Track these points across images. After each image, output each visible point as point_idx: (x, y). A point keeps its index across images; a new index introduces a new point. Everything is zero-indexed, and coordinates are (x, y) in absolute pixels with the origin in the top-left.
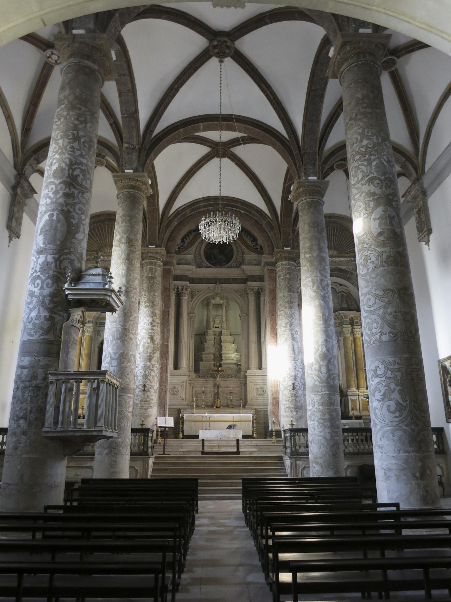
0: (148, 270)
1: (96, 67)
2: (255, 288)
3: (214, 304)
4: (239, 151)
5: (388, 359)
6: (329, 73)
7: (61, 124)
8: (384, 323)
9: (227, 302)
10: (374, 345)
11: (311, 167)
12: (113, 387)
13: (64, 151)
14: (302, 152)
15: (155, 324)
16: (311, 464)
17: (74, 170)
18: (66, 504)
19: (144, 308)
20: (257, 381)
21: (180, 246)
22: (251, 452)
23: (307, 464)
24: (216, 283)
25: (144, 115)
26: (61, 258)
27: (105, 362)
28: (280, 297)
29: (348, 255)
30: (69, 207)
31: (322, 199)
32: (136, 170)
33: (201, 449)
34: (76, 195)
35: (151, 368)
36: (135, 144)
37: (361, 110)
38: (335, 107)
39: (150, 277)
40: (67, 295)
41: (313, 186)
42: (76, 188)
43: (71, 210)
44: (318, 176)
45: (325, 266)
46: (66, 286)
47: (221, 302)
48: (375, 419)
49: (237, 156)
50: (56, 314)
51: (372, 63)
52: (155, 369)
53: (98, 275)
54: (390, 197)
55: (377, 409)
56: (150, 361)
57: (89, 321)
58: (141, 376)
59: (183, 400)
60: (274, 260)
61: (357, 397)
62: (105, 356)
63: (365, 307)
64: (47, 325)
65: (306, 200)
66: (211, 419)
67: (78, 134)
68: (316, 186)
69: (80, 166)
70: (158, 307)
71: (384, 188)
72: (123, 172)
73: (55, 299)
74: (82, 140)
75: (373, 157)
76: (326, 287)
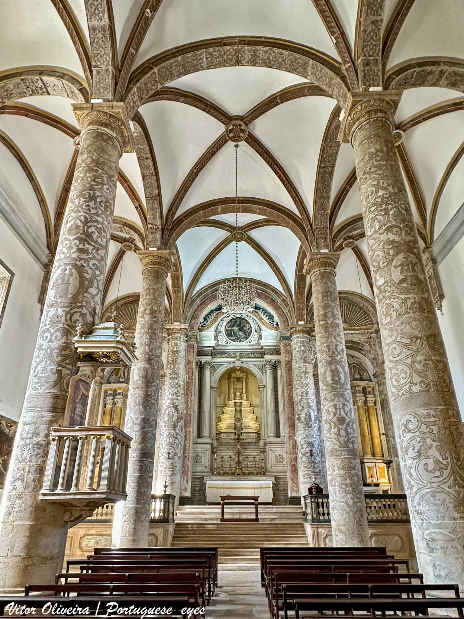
0: (173, 344)
1: (114, 135)
3: (235, 378)
4: (255, 234)
5: (421, 411)
6: (340, 138)
7: (78, 184)
8: (414, 373)
9: (247, 376)
10: (403, 397)
13: (80, 209)
14: (313, 228)
15: (179, 394)
16: (333, 533)
17: (89, 227)
18: (82, 572)
22: (272, 519)
23: (329, 532)
25: (167, 199)
26: (72, 312)
27: (127, 428)
28: (296, 368)
29: (359, 328)
30: (82, 262)
31: (335, 271)
33: (220, 516)
34: (90, 251)
35: (175, 436)
36: (158, 224)
37: (375, 163)
39: (175, 351)
40: (76, 349)
41: (325, 258)
42: (90, 244)
43: (85, 265)
45: (339, 332)
46: (76, 338)
47: (242, 375)
48: (410, 479)
50: (63, 367)
51: (384, 120)
52: (179, 437)
53: (110, 328)
54: (411, 244)
55: (412, 468)
56: (174, 430)
57: (119, 394)
63: (391, 357)
64: (54, 378)
67: (94, 194)
68: (328, 258)
69: (96, 224)
70: (183, 379)
71: (403, 235)
72: (147, 249)
73: (63, 352)
74: (98, 200)
75: (390, 207)
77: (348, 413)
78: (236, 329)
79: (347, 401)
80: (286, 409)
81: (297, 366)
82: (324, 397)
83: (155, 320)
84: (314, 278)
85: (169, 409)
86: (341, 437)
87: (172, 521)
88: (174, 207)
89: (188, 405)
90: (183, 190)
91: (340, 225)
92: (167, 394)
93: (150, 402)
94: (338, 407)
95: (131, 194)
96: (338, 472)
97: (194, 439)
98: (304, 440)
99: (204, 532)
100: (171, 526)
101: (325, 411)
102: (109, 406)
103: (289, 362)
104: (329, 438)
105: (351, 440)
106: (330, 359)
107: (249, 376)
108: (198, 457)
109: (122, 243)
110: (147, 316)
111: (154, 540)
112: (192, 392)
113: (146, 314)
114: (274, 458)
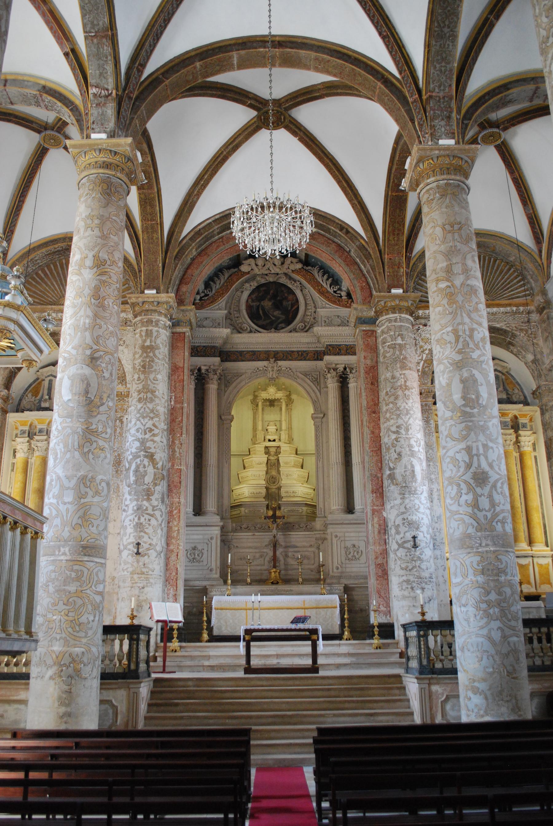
0: (143, 334)
2: (338, 366)
3: (266, 400)
9: (289, 396)
11: (443, 123)
12: (24, 533)
14: (424, 97)
15: (156, 431)
19: (138, 404)
20: (347, 534)
21: (203, 295)
24: (267, 359)
27: (51, 495)
28: (386, 379)
31: (467, 182)
32: (112, 135)
33: (243, 662)
35: (150, 511)
38: (483, 12)
39: (148, 347)
41: (448, 156)
44: (456, 137)
47: (280, 395)
49: (302, 125)
52: (158, 513)
56: (149, 500)
58: (132, 525)
59: (211, 570)
60: (372, 313)
61: (530, 559)
62: (50, 483)
65: (435, 184)
66: (263, 605)
70: (163, 401)
72: (88, 137)
76: (481, 344)
77: (494, 464)
78: (267, 304)
79: (491, 441)
80: (367, 458)
81: (389, 375)
82: (445, 433)
83: (104, 278)
84: (426, 196)
85: (138, 460)
86: (479, 510)
87: (146, 675)
88: (143, 53)
89: (174, 451)
90: (161, 20)
91: (478, 91)
92: (133, 431)
93: (95, 445)
94: (474, 452)
95: (55, 26)
96: (474, 579)
97: (187, 518)
98: (400, 518)
99: (209, 694)
100: (142, 685)
101: (448, 460)
102: (20, 456)
103: (373, 367)
104: (457, 513)
105: (500, 517)
106: (458, 357)
107: (294, 397)
108: (197, 552)
109: (39, 132)
110: (88, 270)
111: (110, 711)
112: (181, 428)
113: (85, 268)
114: (343, 552)
